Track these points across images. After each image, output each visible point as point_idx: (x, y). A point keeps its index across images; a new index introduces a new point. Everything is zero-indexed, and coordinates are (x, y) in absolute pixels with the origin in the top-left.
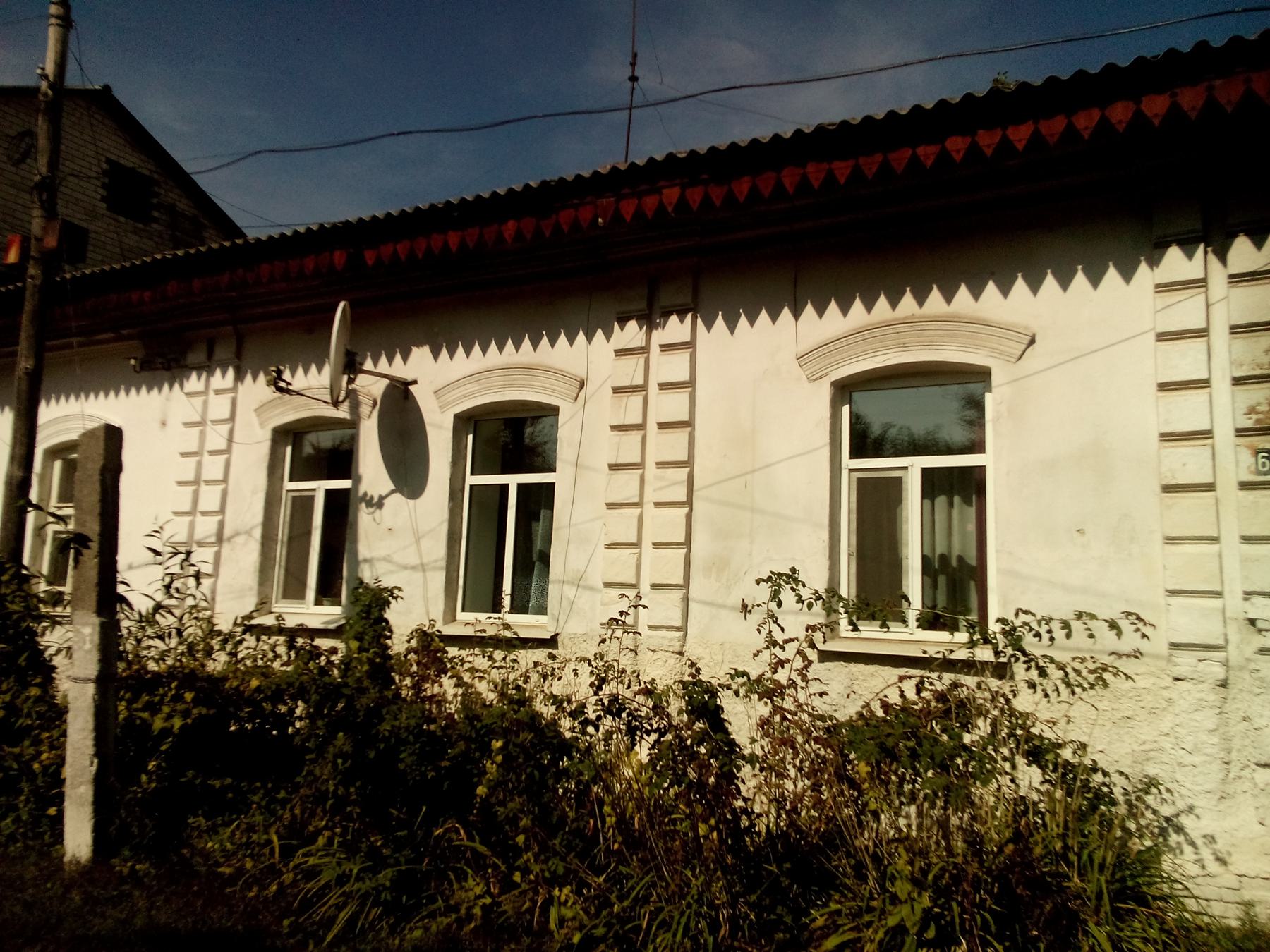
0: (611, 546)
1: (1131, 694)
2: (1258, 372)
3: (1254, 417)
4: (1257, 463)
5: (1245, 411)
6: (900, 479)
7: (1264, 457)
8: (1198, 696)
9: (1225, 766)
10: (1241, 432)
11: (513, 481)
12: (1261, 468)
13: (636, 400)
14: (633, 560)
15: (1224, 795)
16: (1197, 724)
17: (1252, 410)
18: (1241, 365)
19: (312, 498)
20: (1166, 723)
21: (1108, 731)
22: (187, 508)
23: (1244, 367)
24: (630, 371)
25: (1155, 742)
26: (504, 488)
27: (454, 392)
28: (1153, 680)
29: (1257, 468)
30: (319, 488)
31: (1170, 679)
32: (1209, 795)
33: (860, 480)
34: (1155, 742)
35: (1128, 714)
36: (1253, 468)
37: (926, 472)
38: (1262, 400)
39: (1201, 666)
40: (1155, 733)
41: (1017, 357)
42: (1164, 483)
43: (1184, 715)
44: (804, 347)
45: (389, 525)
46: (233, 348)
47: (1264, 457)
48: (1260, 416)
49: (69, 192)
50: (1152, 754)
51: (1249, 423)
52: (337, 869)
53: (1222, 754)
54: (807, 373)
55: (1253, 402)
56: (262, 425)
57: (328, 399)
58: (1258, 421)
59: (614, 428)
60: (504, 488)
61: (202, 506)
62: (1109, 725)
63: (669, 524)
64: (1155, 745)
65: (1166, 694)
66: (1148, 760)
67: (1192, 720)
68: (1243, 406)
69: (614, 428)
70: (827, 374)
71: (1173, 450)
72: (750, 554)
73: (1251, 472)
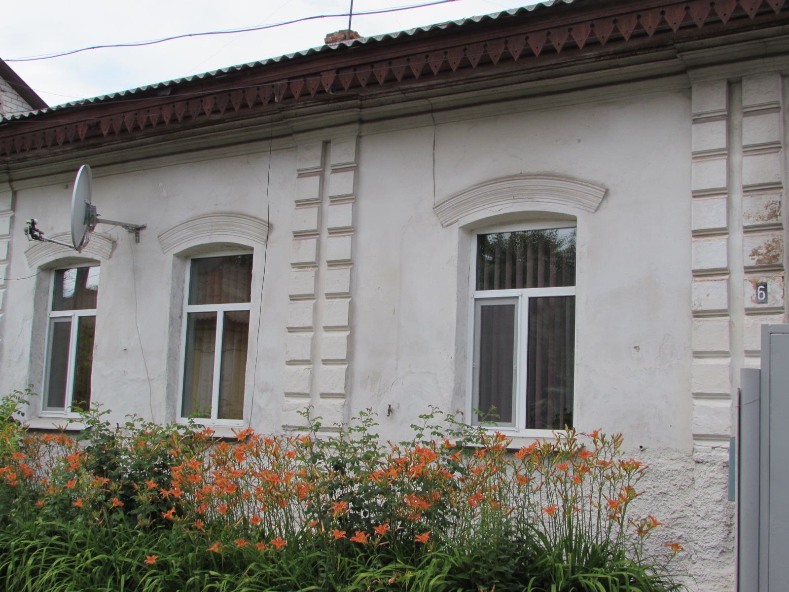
0: (291, 362)
1: (666, 475)
2: (760, 223)
3: (756, 258)
4: (757, 295)
5: (750, 253)
7: (761, 289)
8: (711, 475)
9: (727, 528)
10: (748, 270)
11: (220, 309)
12: (759, 298)
13: (312, 242)
14: (308, 373)
15: (725, 550)
16: (709, 497)
17: (755, 253)
18: (749, 217)
19: (69, 324)
20: (690, 496)
21: (650, 504)
23: (751, 219)
24: (308, 219)
25: (682, 511)
27: (174, 236)
28: (682, 464)
29: (757, 298)
30: (75, 315)
31: (694, 463)
32: (714, 550)
33: (483, 307)
34: (682, 511)
35: (665, 490)
36: (754, 298)
37: (533, 301)
38: (763, 245)
39: (713, 453)
40: (684, 504)
41: (595, 208)
42: (693, 309)
43: (700, 490)
46: (9, 201)
47: (761, 289)
48: (761, 257)
50: (679, 520)
51: (753, 263)
53: (725, 519)
54: (441, 220)
55: (756, 246)
56: (30, 265)
58: (758, 261)
59: (294, 265)
62: (650, 499)
63: (336, 312)
64: (682, 513)
65: (690, 474)
66: (676, 525)
67: (705, 493)
68: (749, 250)
69: (294, 265)
70: (457, 221)
71: (700, 283)
72: (396, 369)
73: (753, 301)
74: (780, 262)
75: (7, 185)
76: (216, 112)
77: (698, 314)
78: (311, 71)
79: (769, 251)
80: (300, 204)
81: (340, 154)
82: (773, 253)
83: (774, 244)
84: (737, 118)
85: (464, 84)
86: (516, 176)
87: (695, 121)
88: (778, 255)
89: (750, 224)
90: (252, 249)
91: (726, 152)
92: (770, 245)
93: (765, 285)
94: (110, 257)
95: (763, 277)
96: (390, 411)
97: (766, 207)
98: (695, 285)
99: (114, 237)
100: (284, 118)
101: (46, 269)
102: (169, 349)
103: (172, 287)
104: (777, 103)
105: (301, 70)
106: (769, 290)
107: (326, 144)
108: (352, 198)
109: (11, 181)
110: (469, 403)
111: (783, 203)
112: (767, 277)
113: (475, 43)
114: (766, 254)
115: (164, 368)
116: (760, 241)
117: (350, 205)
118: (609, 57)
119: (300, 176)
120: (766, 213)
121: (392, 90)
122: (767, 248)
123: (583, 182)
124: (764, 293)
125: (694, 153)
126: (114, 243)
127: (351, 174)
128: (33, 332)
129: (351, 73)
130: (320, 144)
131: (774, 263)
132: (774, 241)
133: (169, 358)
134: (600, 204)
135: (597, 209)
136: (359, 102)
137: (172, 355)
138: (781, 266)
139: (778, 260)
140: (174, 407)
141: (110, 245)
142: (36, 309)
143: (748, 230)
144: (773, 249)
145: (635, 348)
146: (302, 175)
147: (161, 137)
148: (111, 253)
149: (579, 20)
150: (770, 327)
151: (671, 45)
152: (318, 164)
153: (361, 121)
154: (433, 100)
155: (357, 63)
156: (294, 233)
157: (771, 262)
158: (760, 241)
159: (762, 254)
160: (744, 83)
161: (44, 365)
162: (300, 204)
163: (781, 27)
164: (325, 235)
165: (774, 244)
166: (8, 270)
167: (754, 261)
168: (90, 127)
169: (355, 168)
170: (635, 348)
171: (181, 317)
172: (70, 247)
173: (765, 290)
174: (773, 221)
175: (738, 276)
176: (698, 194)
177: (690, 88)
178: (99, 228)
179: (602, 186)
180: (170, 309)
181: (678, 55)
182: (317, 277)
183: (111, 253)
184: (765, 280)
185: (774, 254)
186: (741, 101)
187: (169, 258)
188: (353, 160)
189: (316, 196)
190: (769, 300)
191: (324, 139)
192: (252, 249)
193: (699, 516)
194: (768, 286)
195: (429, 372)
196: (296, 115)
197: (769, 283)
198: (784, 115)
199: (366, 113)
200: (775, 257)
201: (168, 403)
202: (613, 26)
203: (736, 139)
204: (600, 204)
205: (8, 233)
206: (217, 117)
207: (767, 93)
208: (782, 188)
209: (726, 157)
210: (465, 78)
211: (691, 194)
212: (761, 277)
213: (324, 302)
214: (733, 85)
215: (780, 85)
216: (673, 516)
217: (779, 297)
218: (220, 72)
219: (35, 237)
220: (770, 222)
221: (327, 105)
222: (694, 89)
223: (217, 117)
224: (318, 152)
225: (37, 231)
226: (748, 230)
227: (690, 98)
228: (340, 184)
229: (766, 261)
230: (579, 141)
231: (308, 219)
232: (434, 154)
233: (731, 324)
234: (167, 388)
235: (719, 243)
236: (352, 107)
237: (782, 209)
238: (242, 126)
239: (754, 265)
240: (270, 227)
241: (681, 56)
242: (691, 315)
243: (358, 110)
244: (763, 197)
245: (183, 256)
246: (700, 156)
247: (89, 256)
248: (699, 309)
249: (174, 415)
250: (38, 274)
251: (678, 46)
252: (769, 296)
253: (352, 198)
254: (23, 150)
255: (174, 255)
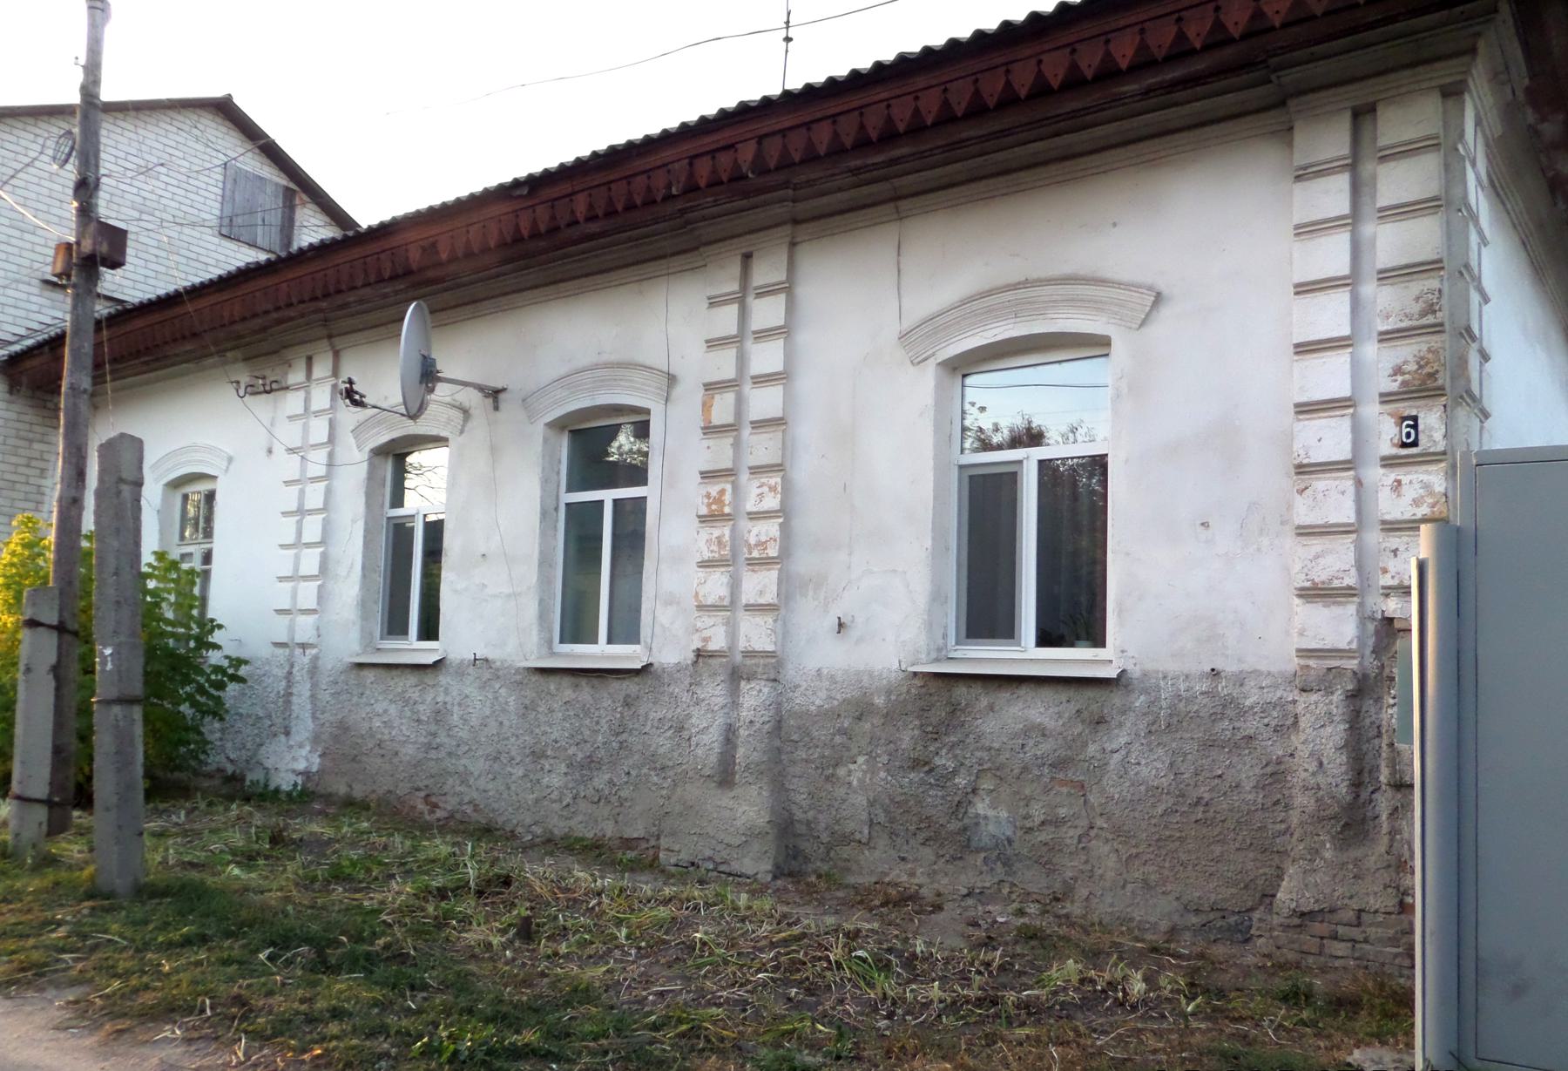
3: (1400, 378)
5: (1391, 371)
6: (1015, 474)
7: (1408, 426)
10: (1386, 398)
11: (608, 496)
17: (1398, 371)
18: (1388, 318)
22: (291, 540)
26: (599, 504)
33: (971, 477)
38: (1410, 358)
44: (907, 324)
45: (483, 550)
47: (1408, 426)
48: (1407, 377)
49: (114, 183)
51: (1394, 386)
52: (715, 548)
55: (1399, 361)
57: (404, 411)
58: (1404, 383)
60: (599, 504)
61: (306, 539)
70: (933, 354)
73: (1394, 445)
74: (1440, 382)
75: (325, 342)
76: (592, 218)
77: (1302, 469)
78: (722, 144)
79: (1421, 367)
80: (713, 344)
81: (767, 271)
82: (1428, 370)
83: (1430, 356)
84: (1367, 168)
85: (944, 152)
86: (1019, 283)
87: (1298, 178)
88: (1437, 371)
89: (1389, 328)
90: (647, 412)
91: (1349, 221)
92: (1422, 358)
93: (1415, 419)
94: (462, 432)
95: (1410, 407)
96: (841, 625)
97: (1417, 299)
98: (1298, 426)
99: (466, 404)
100: (688, 223)
101: (380, 452)
102: (541, 552)
103: (543, 469)
104: (1436, 137)
105: (710, 141)
106: (1421, 427)
107: (747, 257)
108: (784, 331)
109: (330, 337)
110: (951, 615)
111: (1446, 290)
112: (1417, 407)
113: (961, 78)
114: (1416, 371)
115: (534, 578)
116: (1407, 352)
117: (781, 342)
118: (1162, 91)
119: (712, 305)
120: (1416, 308)
121: (837, 171)
122: (1418, 363)
123: (1118, 284)
124: (1412, 431)
125: (1297, 227)
126: (466, 412)
127: (782, 298)
128: (365, 537)
129: (778, 140)
130: (738, 260)
131: (1430, 384)
132: (1429, 350)
133: (541, 564)
134: (1148, 315)
135: (1143, 323)
136: (790, 192)
137: (545, 562)
138: (1442, 388)
139: (1436, 380)
140: (550, 631)
141: (460, 415)
142: (368, 505)
143: (1386, 337)
144: (1427, 363)
145: (1203, 524)
146: (714, 303)
147: (522, 262)
148: (463, 426)
149: (1122, 23)
150: (168, 1011)
151: (1261, 62)
152: (735, 287)
153: (796, 222)
154: (896, 182)
155: (787, 124)
156: (705, 385)
157: (1424, 383)
158: (1407, 352)
159: (1409, 373)
160: (1379, 113)
161: (380, 581)
162: (713, 344)
163: (1445, 13)
164: (746, 432)
165: (1430, 356)
166: (331, 455)
167: (1397, 384)
168: (424, 249)
169: (787, 288)
170: (1203, 524)
171: (556, 509)
172: (403, 415)
173: (1415, 427)
174: (1430, 319)
175: (1371, 410)
176: (1303, 289)
177: (1291, 129)
178: (442, 391)
179: (1150, 288)
180: (542, 497)
181: (1273, 77)
182: (737, 445)
183: (463, 426)
184: (1414, 413)
185: (1431, 371)
186: (1375, 139)
187: (539, 429)
188: (783, 277)
189: (734, 331)
190: (1421, 443)
191: (744, 250)
192: (647, 412)
193: (1306, 770)
194: (1420, 421)
195: (894, 571)
196: (704, 219)
197: (1421, 415)
198: (1445, 155)
199: (803, 208)
200: (1432, 375)
201: (541, 625)
202: (1174, 29)
203: (1365, 199)
204: (1148, 315)
205: (328, 406)
206: (594, 227)
207: (1418, 123)
208: (1443, 268)
209: (1350, 228)
210: (943, 143)
211: (1292, 290)
212: (1408, 409)
213: (744, 524)
214: (1363, 115)
215: (1441, 109)
216: (1264, 771)
217: (1438, 435)
218: (595, 154)
219: (356, 403)
220: (1425, 321)
221: (745, 201)
222: (1298, 125)
223: (594, 227)
224: (735, 269)
225: (357, 393)
226: (1386, 337)
227: (1290, 144)
228: (767, 312)
229: (1417, 383)
230: (1115, 225)
231: (723, 365)
232: (898, 263)
233: (1359, 483)
234: (540, 604)
235: (1341, 360)
236: (782, 200)
237: (1444, 301)
238: (630, 240)
239: (1396, 389)
240: (672, 379)
241: (1278, 77)
242: (1293, 471)
243: (791, 204)
244: (1411, 284)
245: (559, 425)
246: (1306, 230)
247: (434, 432)
248: (1306, 461)
249: (550, 642)
250: (370, 459)
251: (1274, 61)
252: (1421, 437)
253: (784, 331)
254: (339, 292)
255: (547, 425)
